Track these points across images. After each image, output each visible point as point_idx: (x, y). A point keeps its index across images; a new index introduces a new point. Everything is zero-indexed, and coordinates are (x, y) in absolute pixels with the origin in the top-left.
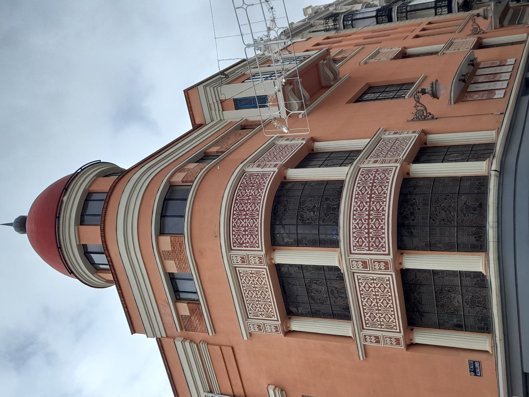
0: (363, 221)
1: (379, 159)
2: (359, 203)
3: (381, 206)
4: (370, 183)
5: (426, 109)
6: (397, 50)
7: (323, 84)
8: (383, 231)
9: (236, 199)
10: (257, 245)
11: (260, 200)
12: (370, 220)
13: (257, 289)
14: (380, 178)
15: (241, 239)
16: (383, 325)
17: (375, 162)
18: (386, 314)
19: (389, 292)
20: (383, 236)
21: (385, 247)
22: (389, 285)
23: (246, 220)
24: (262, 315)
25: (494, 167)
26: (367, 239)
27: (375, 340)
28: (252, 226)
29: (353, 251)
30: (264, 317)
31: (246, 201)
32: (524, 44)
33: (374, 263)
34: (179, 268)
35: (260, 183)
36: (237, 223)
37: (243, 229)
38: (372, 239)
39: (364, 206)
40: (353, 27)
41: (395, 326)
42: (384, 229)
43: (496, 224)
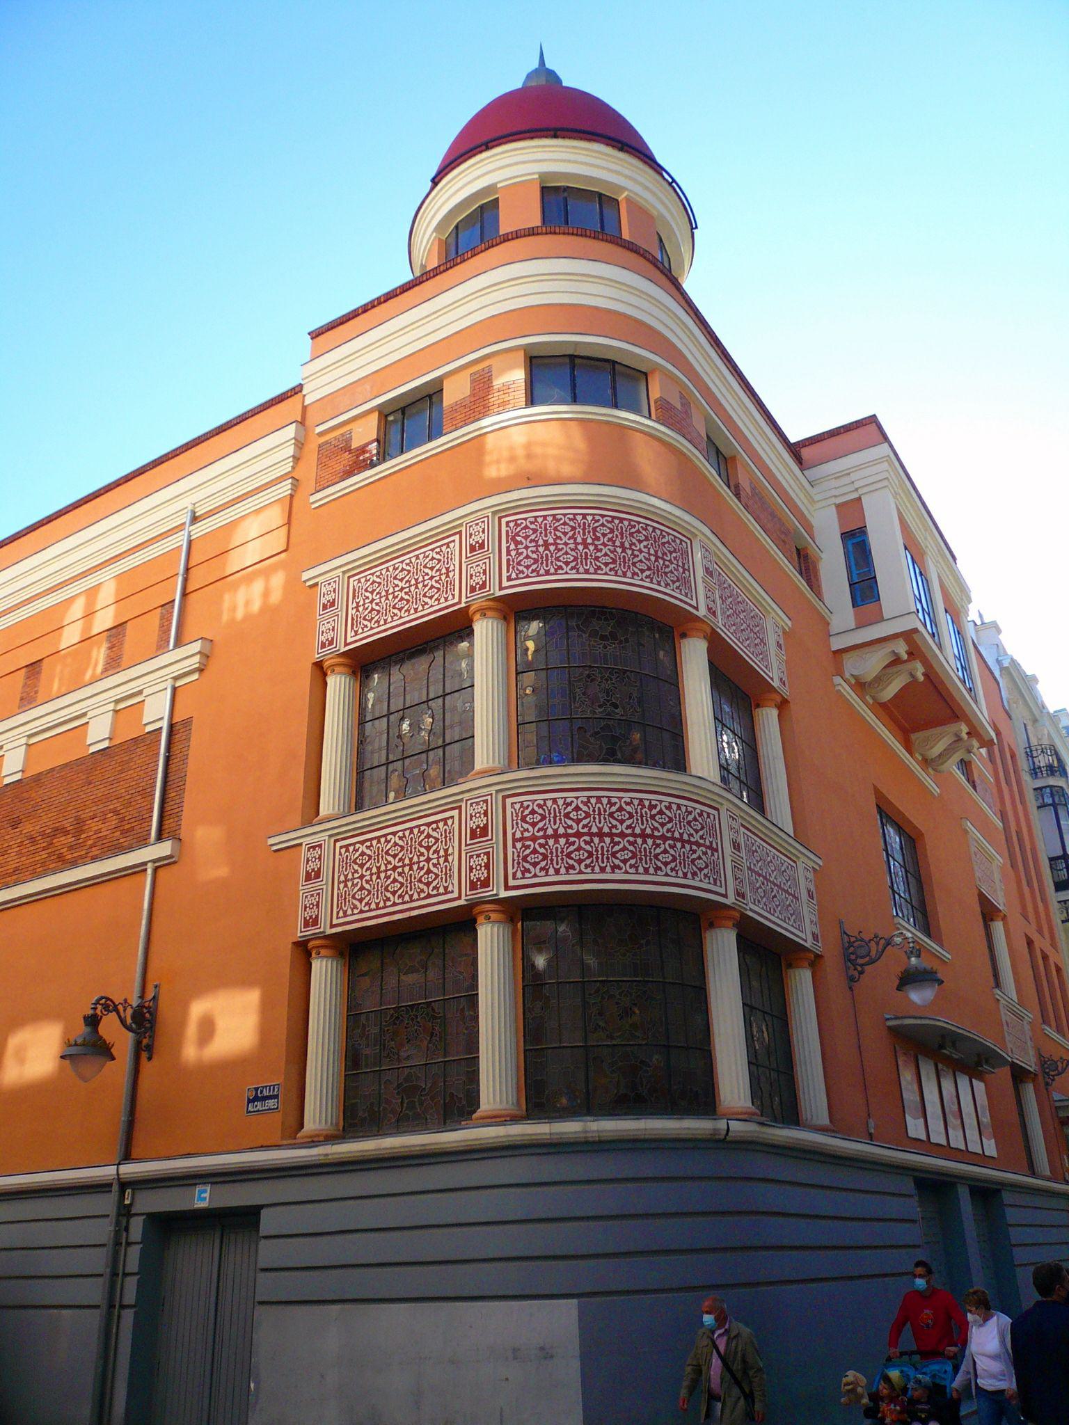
2: (628, 808)
3: (625, 861)
4: (681, 835)
5: (872, 962)
6: (999, 900)
7: (913, 737)
8: (563, 870)
9: (622, 520)
10: (514, 576)
11: (625, 575)
12: (587, 838)
14: (694, 856)
15: (526, 537)
16: (346, 886)
17: (736, 846)
18: (369, 892)
20: (551, 871)
21: (524, 878)
22: (435, 892)
23: (573, 546)
24: (357, 608)
25: (735, 1125)
26: (541, 833)
29: (509, 801)
30: (351, 612)
31: (618, 543)
32: (1029, 1173)
34: (453, 409)
35: (666, 574)
36: (565, 524)
37: (551, 541)
38: (541, 845)
39: (622, 822)
40: (1039, 807)
42: (567, 873)
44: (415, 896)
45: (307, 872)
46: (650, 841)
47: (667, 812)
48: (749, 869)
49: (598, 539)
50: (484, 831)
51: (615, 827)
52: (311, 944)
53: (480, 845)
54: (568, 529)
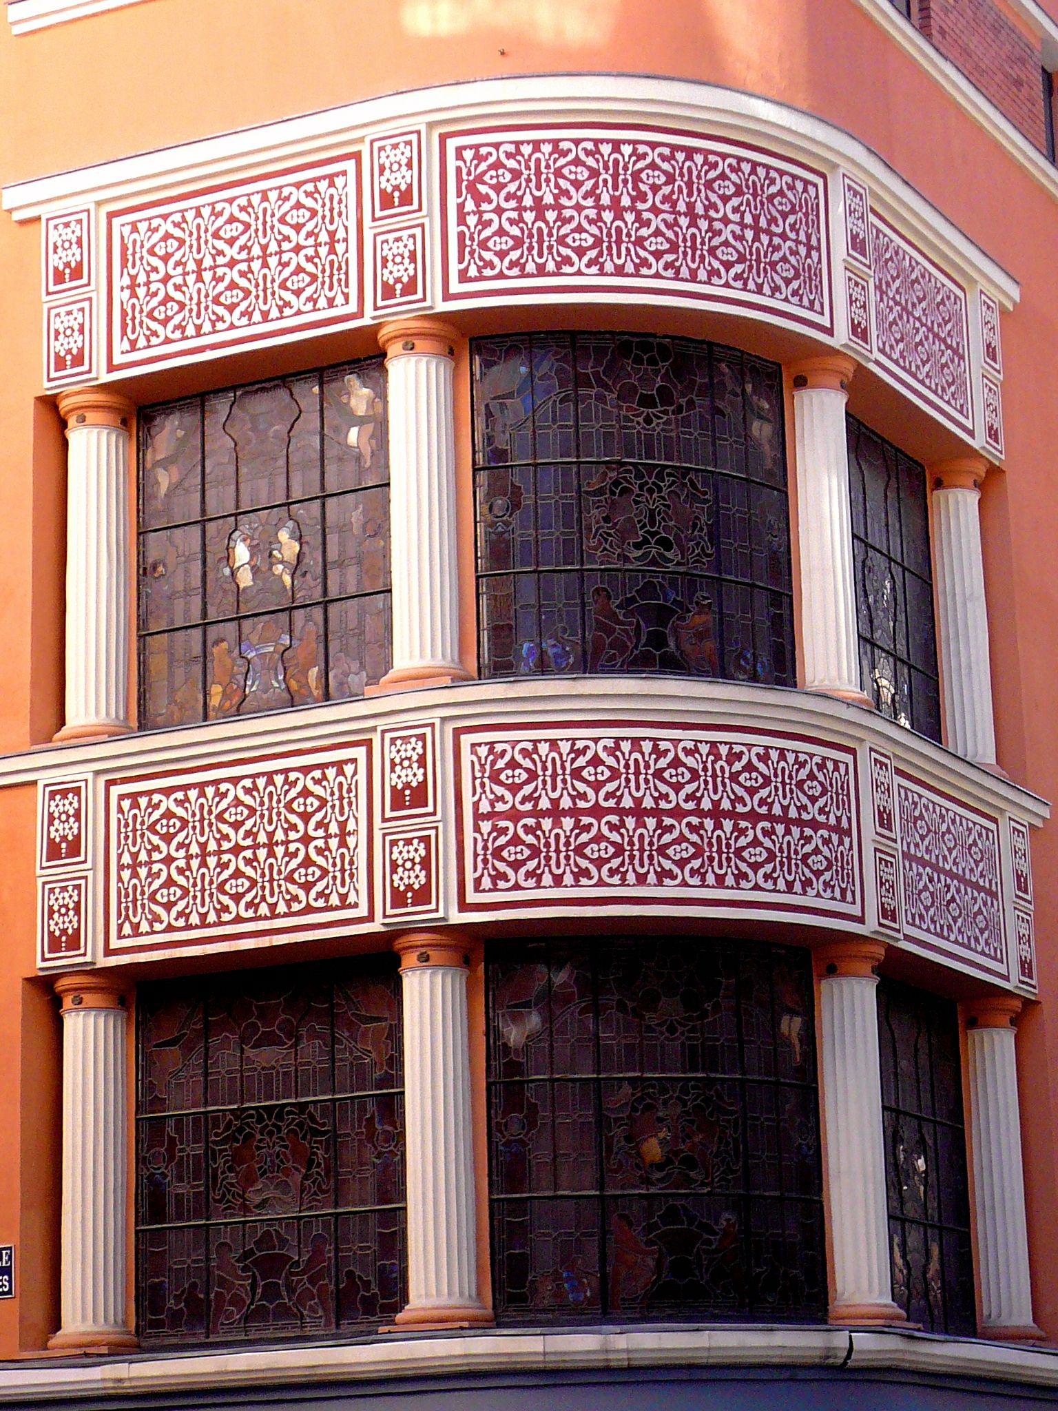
0: (610, 787)
1: (897, 834)
2: (690, 761)
3: (682, 863)
4: (785, 809)
8: (568, 879)
9: (690, 152)
10: (473, 272)
11: (693, 278)
12: (614, 819)
13: (256, 265)
14: (808, 849)
15: (498, 188)
16: (135, 875)
17: (884, 819)
19: (288, 903)
20: (547, 879)
21: (495, 889)
22: (321, 903)
24: (133, 287)
26: (528, 806)
27: (64, 931)
28: (561, 241)
31: (681, 207)
33: (421, 839)
35: (773, 265)
36: (577, 162)
37: (549, 199)
39: (677, 787)
41: (136, 927)
43: (618, 1360)
44: (282, 908)
45: (51, 841)
46: (728, 825)
47: (761, 767)
48: (906, 855)
49: (642, 197)
50: (419, 795)
51: (665, 797)
52: (62, 984)
53: (412, 823)
54: (583, 174)
